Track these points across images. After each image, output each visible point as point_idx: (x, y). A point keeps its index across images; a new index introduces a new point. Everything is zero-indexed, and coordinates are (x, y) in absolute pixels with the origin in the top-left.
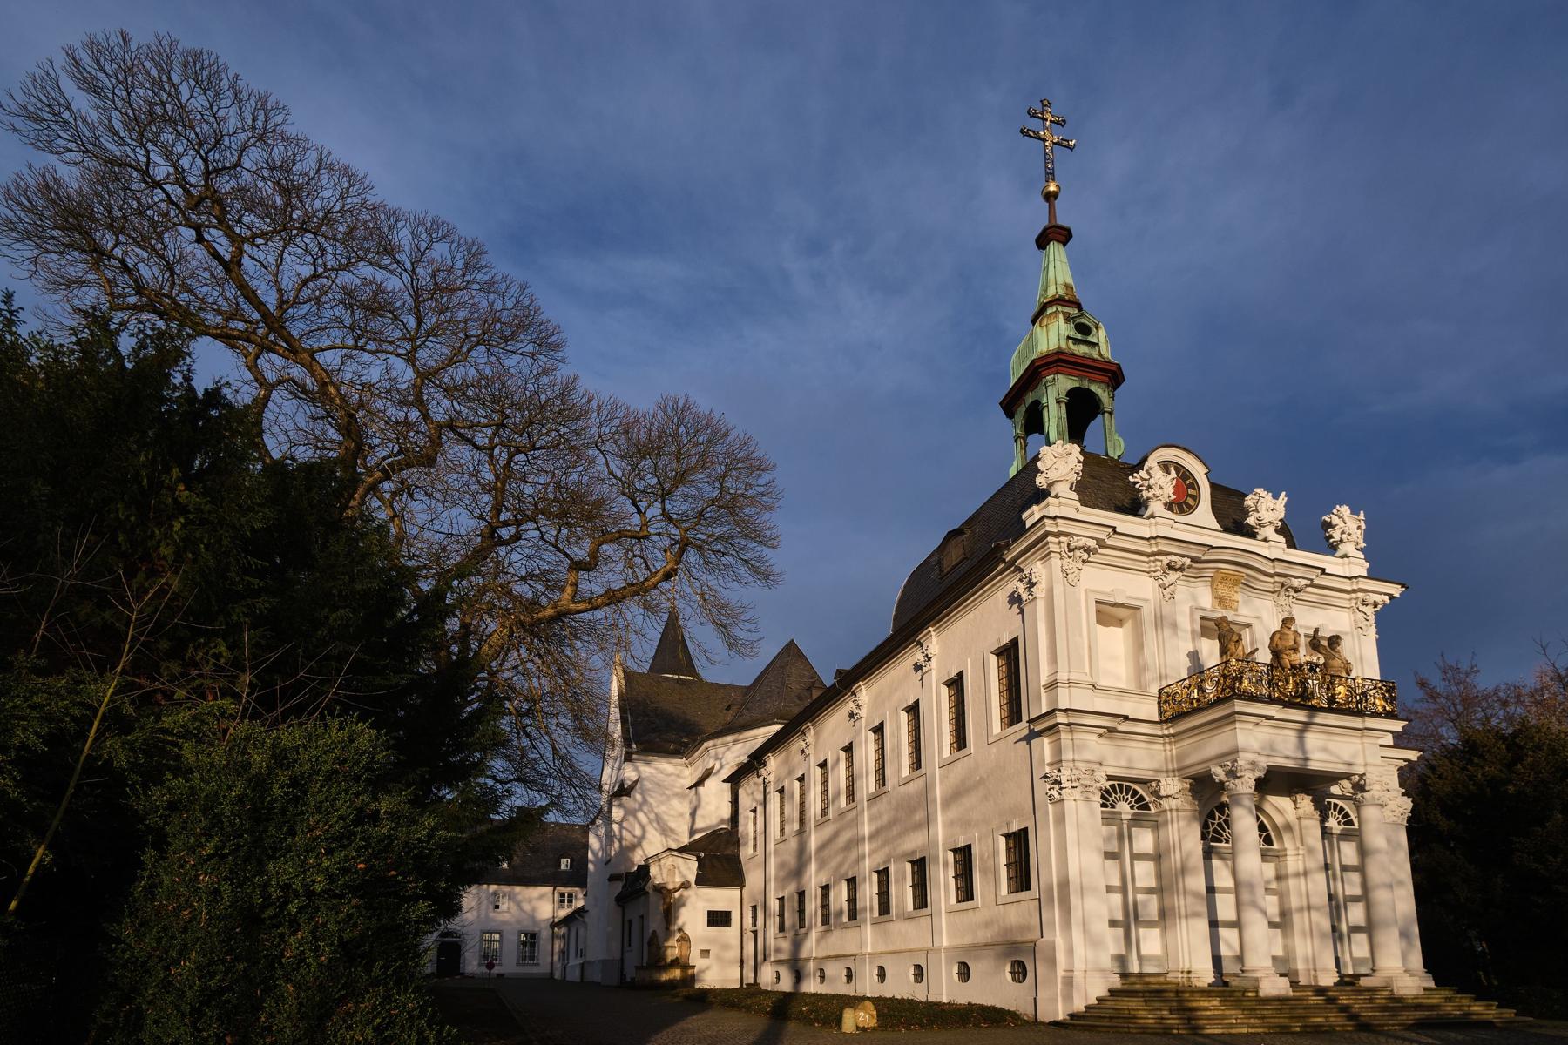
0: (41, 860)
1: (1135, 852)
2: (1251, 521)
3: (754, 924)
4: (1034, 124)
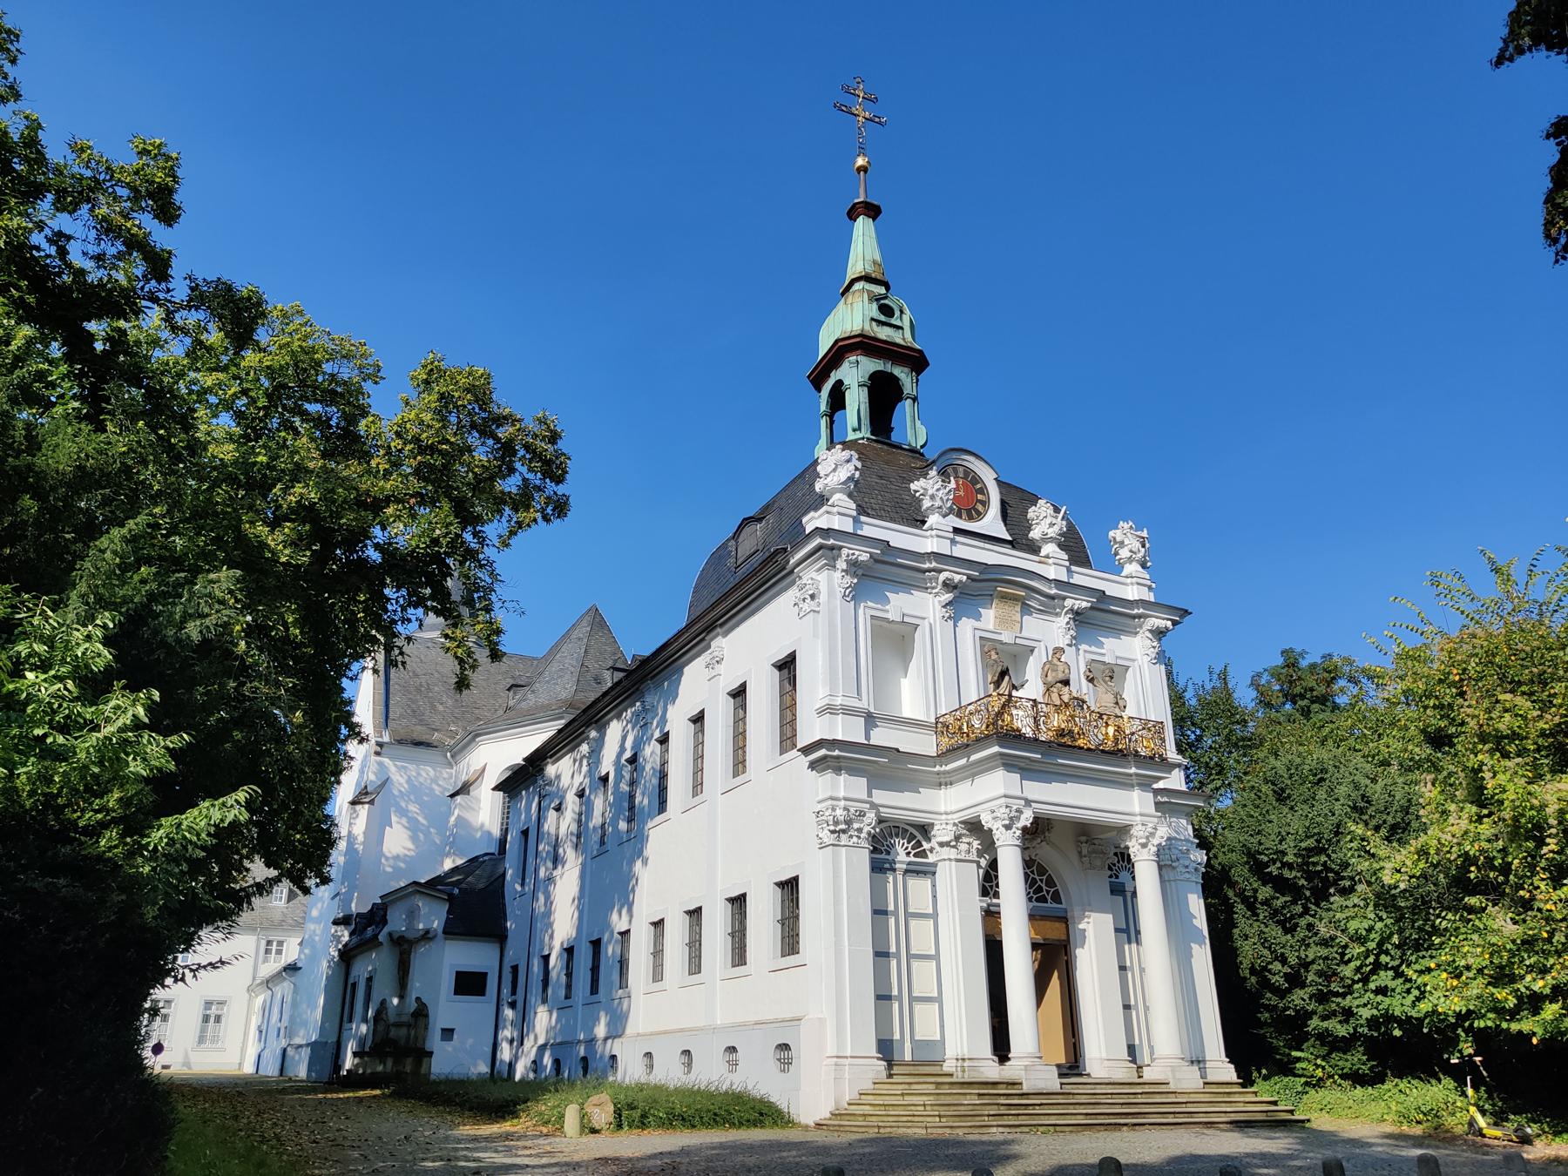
1: (1121, 898)
2: (1035, 534)
3: (514, 992)
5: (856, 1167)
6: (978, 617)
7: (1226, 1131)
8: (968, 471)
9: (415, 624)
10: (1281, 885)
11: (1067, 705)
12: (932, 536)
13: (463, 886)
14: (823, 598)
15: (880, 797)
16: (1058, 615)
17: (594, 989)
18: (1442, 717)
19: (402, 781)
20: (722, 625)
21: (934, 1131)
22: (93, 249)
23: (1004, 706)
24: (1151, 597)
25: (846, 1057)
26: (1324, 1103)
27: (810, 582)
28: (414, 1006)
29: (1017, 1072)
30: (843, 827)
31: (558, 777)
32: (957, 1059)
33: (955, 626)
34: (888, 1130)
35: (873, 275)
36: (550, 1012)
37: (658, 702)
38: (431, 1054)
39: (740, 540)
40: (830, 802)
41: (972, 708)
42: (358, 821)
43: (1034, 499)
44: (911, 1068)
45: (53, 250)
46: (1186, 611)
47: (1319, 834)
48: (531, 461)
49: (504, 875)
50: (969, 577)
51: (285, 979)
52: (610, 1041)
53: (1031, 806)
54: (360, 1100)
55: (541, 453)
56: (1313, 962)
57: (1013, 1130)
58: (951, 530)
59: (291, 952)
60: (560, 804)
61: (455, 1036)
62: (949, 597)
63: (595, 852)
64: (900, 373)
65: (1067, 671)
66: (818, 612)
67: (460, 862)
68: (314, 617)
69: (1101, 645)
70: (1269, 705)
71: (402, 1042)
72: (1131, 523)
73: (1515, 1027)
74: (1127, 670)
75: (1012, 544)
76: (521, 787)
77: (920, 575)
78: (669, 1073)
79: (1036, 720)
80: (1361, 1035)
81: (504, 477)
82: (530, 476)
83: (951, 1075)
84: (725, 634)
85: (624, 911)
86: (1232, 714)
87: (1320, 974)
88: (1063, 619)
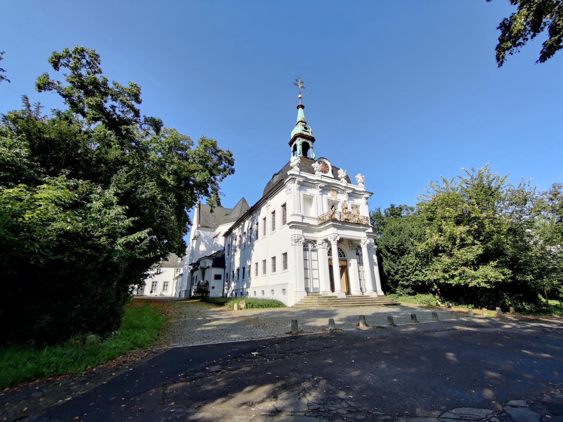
0: (558, 319)
2: (339, 176)
3: (227, 279)
4: (297, 82)
5: (300, 317)
6: (327, 194)
8: (324, 163)
9: (201, 198)
10: (393, 253)
11: (347, 213)
14: (292, 190)
15: (305, 234)
16: (345, 194)
17: (244, 278)
18: (432, 214)
20: (269, 198)
22: (121, 110)
23: (333, 213)
24: (365, 190)
30: (297, 241)
31: (235, 233)
36: (235, 283)
38: (209, 292)
41: (326, 214)
45: (112, 110)
48: (225, 160)
49: (225, 254)
50: (325, 185)
54: (193, 302)
56: (400, 269)
59: (182, 272)
61: (215, 288)
62: (321, 190)
64: (309, 142)
67: (216, 252)
68: (179, 197)
69: (354, 201)
71: (203, 289)
73: (449, 282)
77: (314, 185)
78: (259, 296)
81: (220, 165)
82: (225, 164)
84: (270, 200)
85: (250, 261)
87: (402, 272)
88: (346, 195)
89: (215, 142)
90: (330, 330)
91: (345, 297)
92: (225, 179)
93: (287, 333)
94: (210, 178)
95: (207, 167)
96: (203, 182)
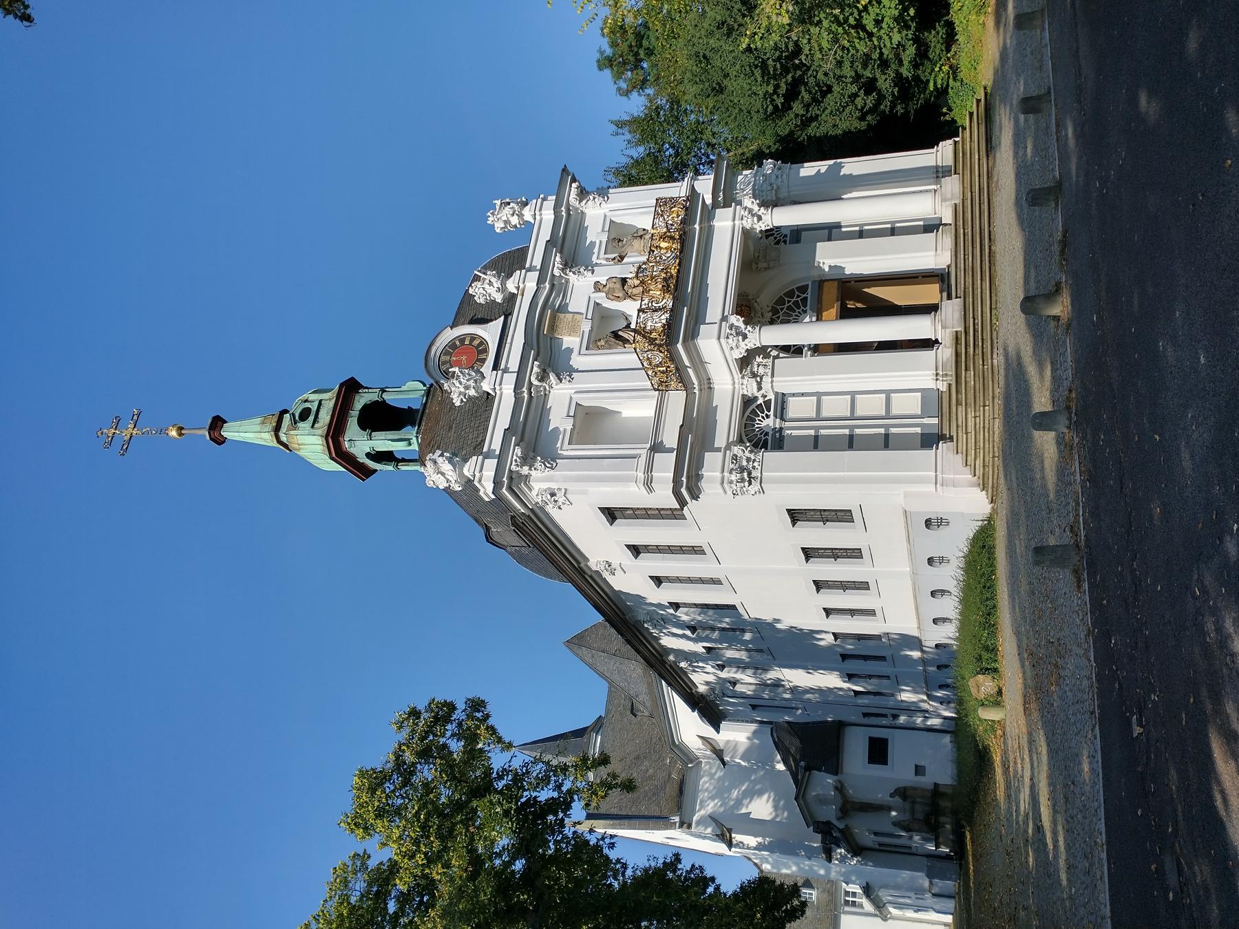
2: (499, 298)
3: (885, 716)
4: (117, 445)
6: (570, 351)
7: (995, 161)
8: (445, 352)
10: (791, 95)
11: (642, 282)
12: (501, 389)
13: (798, 757)
14: (554, 486)
16: (567, 281)
17: (883, 658)
19: (712, 805)
20: (578, 563)
21: (996, 411)
23: (644, 337)
25: (936, 476)
26: (970, 66)
27: (540, 497)
28: (897, 799)
29: (947, 335)
30: (745, 474)
31: (707, 683)
32: (937, 380)
33: (578, 371)
34: (996, 449)
35: (274, 424)
37: (645, 609)
38: (936, 785)
39: (506, 544)
40: (725, 485)
42: (746, 843)
43: (468, 298)
44: (944, 418)
46: (563, 170)
47: (750, 66)
49: (788, 723)
51: (877, 895)
52: (924, 648)
53: (727, 316)
55: (428, 726)
56: (856, 72)
57: (995, 345)
58: (495, 372)
59: (855, 888)
60: (730, 682)
61: (923, 763)
62: (552, 377)
63: (770, 657)
64: (361, 401)
65: (614, 280)
66: (566, 490)
69: (593, 244)
70: (644, 81)
72: (489, 214)
74: (613, 221)
75: (508, 315)
76: (716, 710)
77: (534, 401)
78: (949, 607)
79: (656, 310)
80: (914, 34)
81: (451, 753)
83: (950, 385)
84: (587, 560)
85: (818, 636)
86: (652, 119)
87: (865, 66)
88: (572, 277)
89: (363, 774)
90: (1069, 428)
91: (959, 301)
92: (502, 731)
93: (1079, 587)
94: (501, 792)
95: (458, 806)
96: (518, 819)
